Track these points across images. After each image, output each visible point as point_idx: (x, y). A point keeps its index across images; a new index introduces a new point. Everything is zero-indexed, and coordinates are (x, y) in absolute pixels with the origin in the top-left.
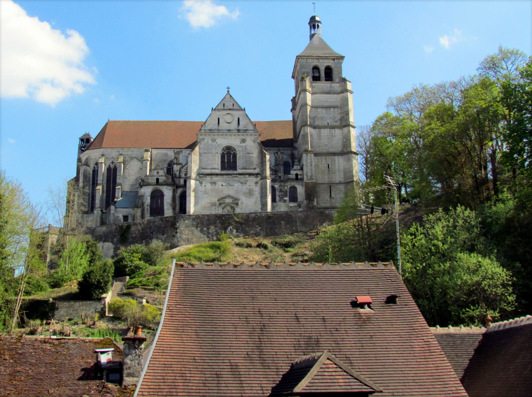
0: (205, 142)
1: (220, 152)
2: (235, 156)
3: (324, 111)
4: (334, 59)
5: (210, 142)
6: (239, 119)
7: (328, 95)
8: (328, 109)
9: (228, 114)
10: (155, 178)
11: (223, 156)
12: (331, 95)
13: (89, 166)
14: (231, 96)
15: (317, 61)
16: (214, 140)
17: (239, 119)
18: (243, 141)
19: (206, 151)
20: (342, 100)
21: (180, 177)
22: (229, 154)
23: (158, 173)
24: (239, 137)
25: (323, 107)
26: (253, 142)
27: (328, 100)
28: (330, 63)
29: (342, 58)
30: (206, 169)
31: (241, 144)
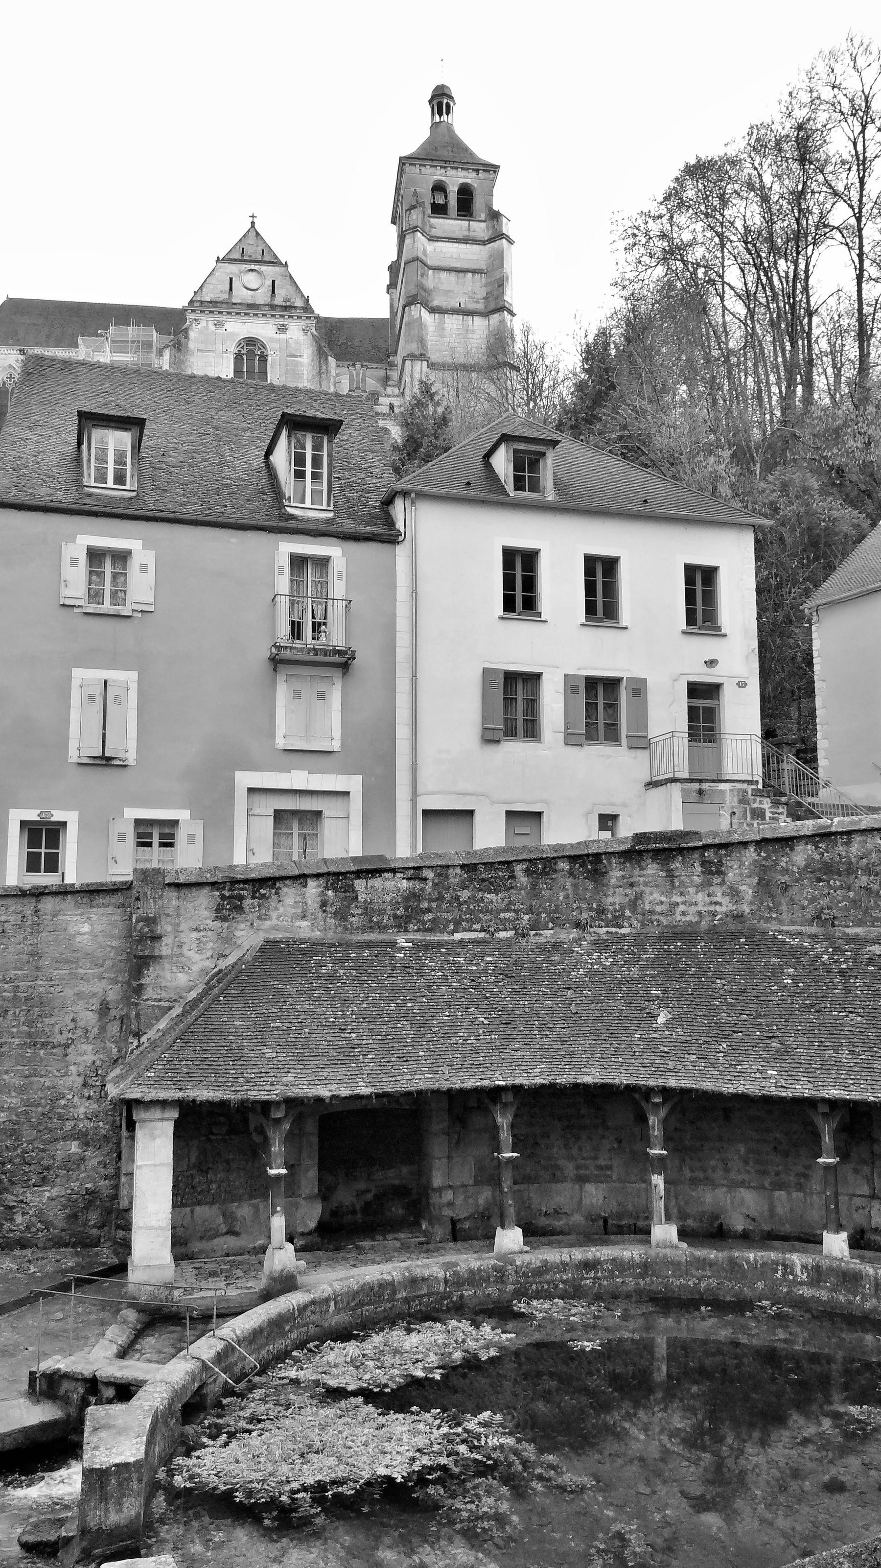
0: (199, 326)
1: (233, 349)
2: (263, 359)
3: (453, 276)
5: (212, 327)
6: (273, 282)
9: (252, 270)
11: (238, 357)
14: (258, 234)
16: (219, 324)
17: (273, 282)
18: (283, 329)
19: (202, 347)
20: (490, 256)
22: (251, 353)
24: (272, 321)
25: (450, 270)
26: (302, 333)
27: (462, 256)
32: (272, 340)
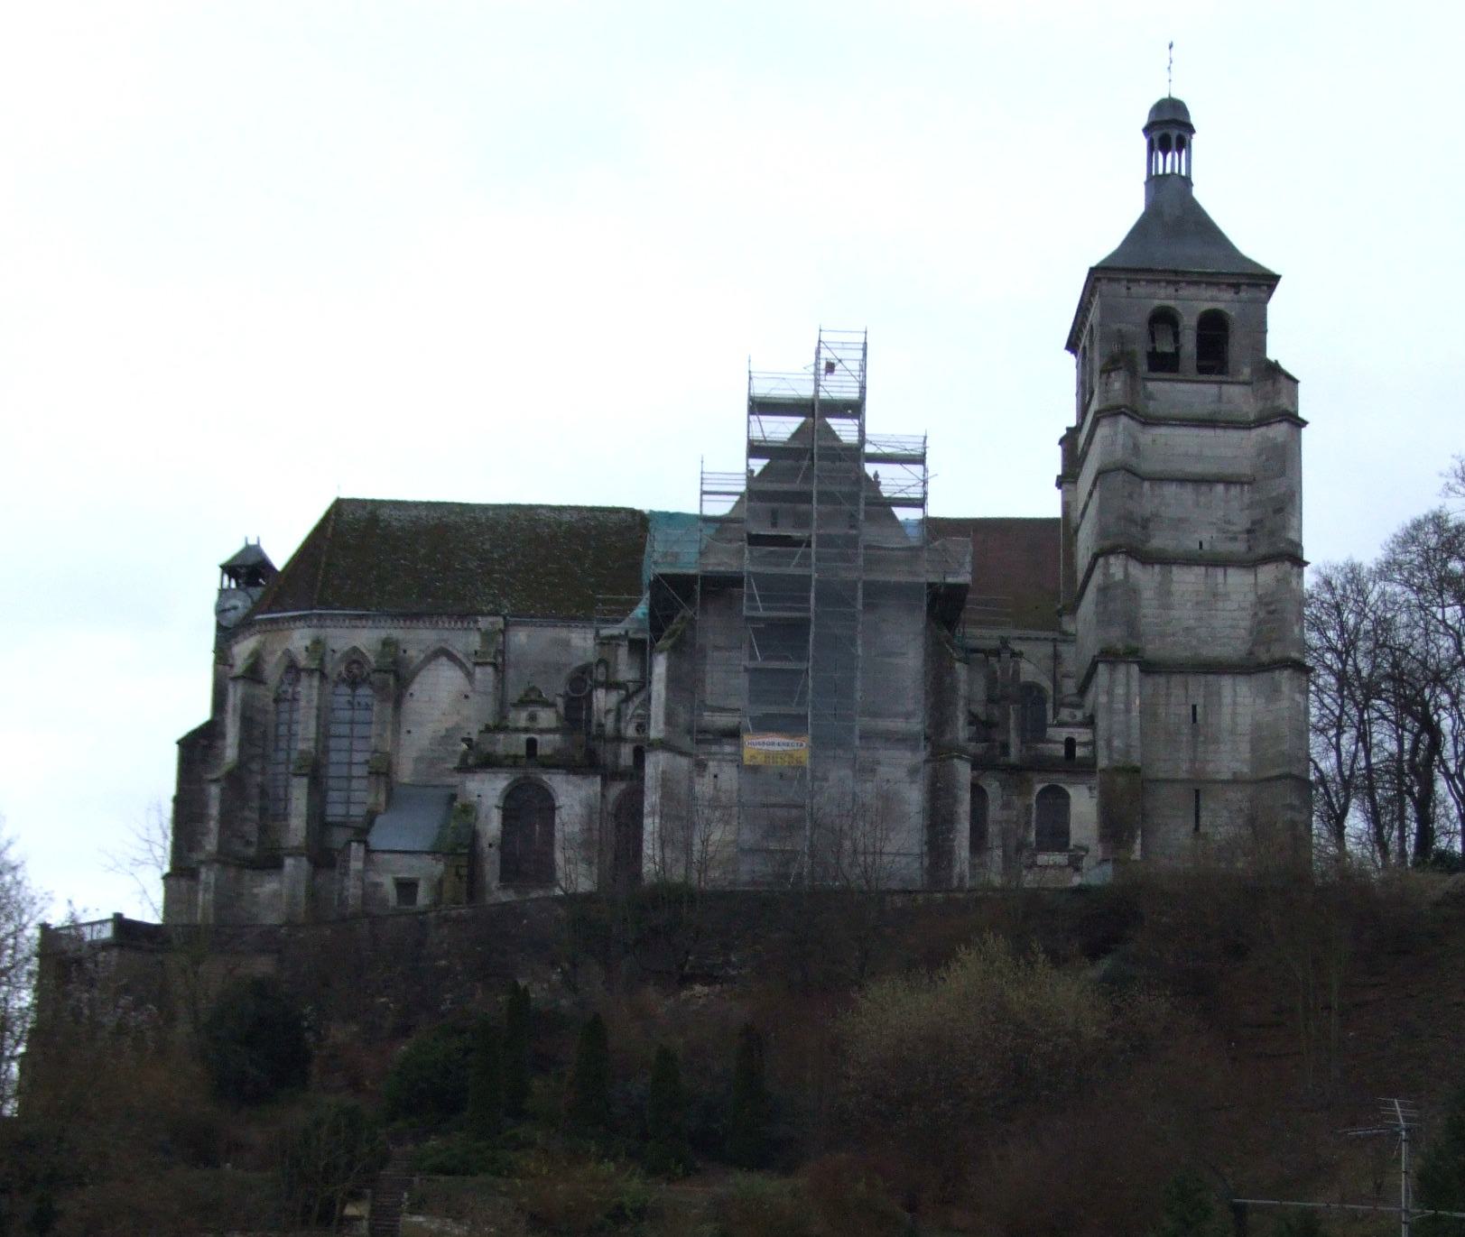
3: (1187, 493)
4: (1236, 287)
7: (1208, 433)
8: (1204, 488)
10: (524, 737)
12: (1219, 432)
13: (261, 682)
15: (1171, 290)
21: (619, 738)
23: (533, 718)
25: (1182, 480)
28: (1223, 301)
29: (1276, 278)
30: (722, 710)
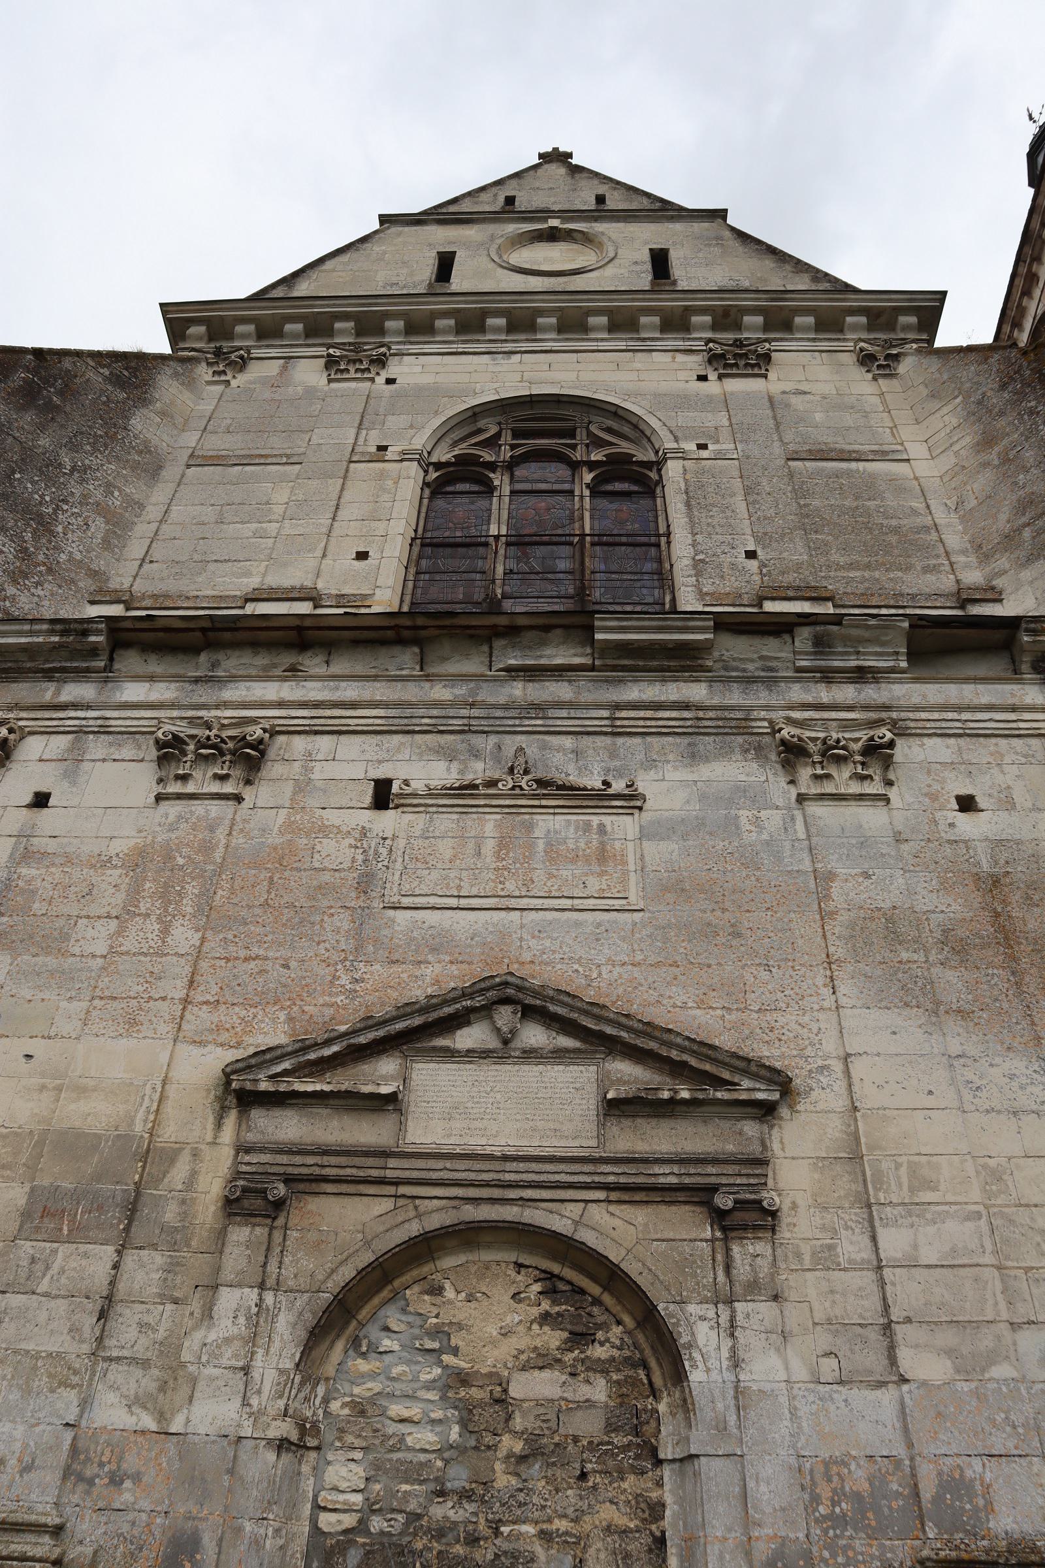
31: (713, 387)
32: (683, 401)
